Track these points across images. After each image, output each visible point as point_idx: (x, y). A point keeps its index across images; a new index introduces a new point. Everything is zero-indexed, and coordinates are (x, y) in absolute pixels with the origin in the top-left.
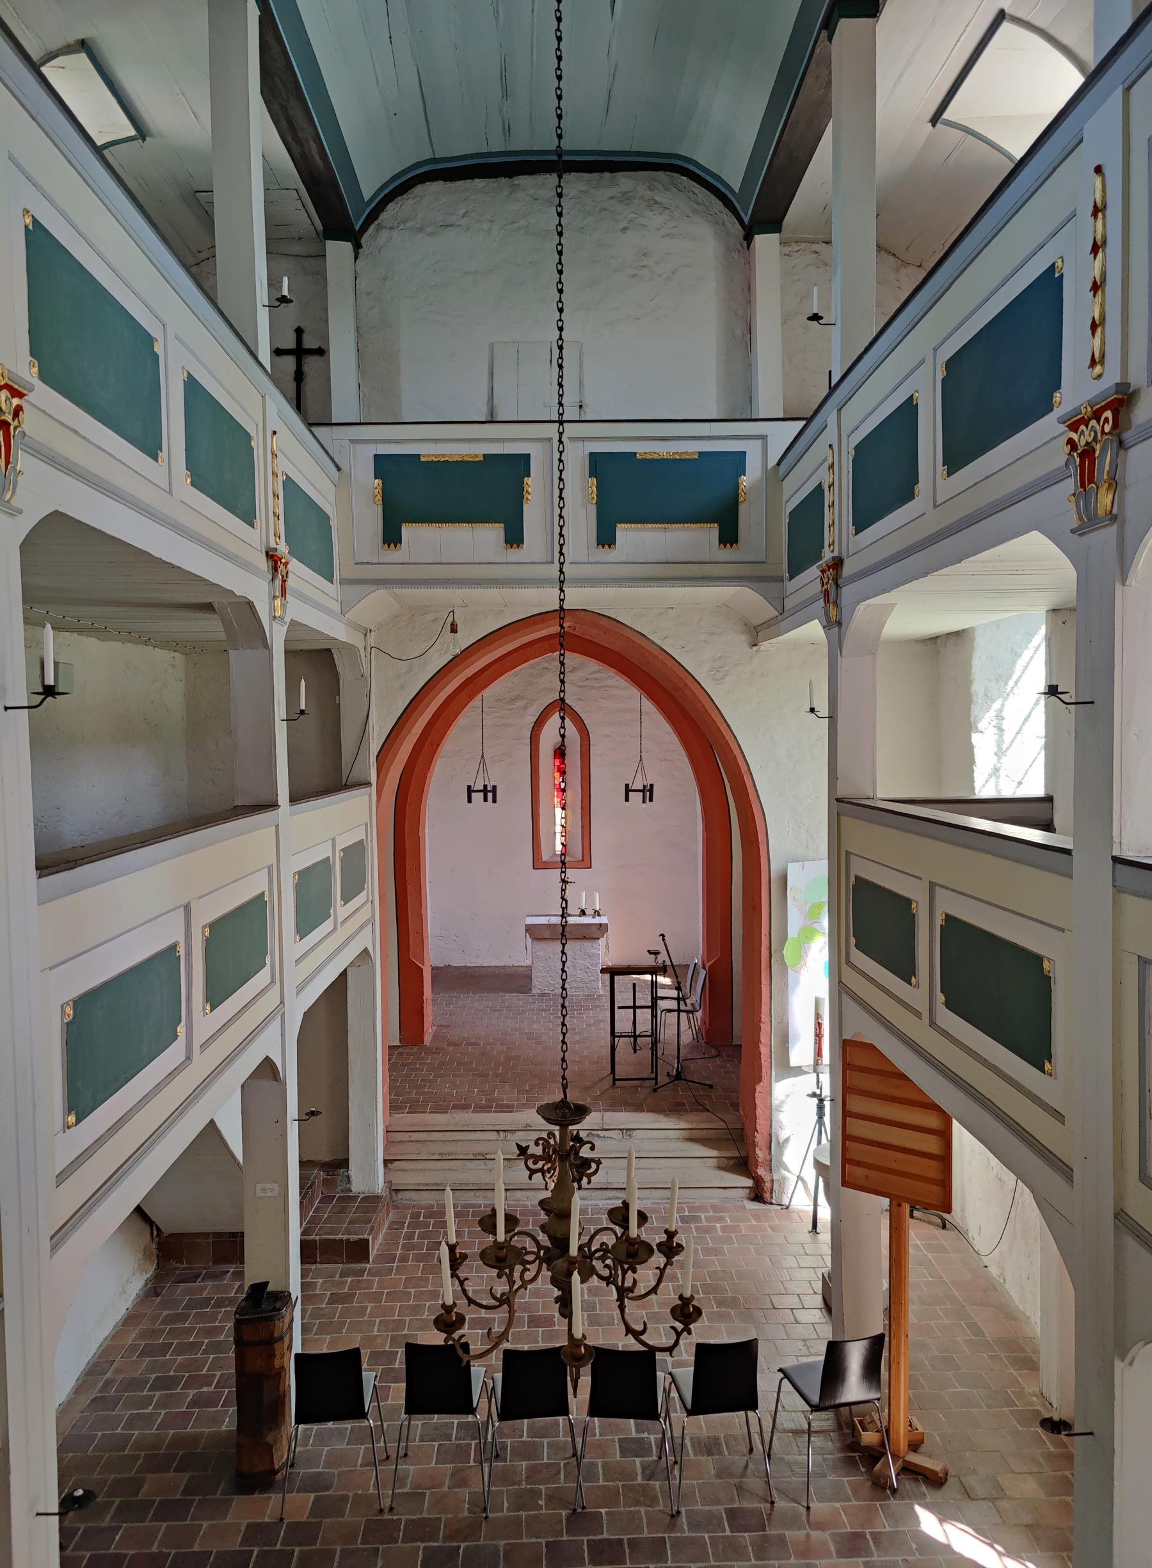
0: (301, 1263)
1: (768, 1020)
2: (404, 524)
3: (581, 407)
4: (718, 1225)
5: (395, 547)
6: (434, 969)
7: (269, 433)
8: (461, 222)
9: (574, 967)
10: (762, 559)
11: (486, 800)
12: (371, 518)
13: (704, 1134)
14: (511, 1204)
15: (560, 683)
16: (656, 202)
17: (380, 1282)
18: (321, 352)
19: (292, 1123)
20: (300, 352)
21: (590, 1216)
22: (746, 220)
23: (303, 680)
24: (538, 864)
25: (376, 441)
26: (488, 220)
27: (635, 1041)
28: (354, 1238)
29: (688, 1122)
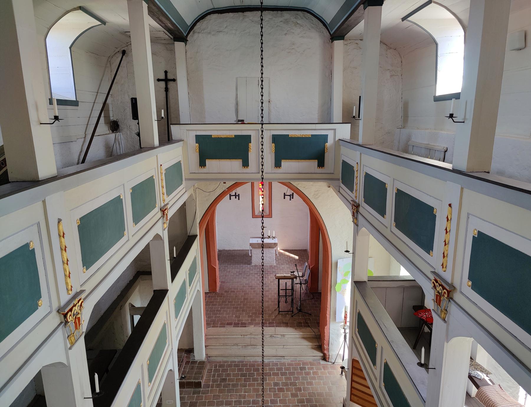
0: (180, 388)
1: (330, 307)
2: (207, 160)
3: (269, 102)
4: (311, 371)
5: (204, 167)
6: (219, 251)
7: (159, 166)
8: (225, 30)
9: (266, 257)
10: (332, 172)
11: (236, 198)
12: (195, 157)
13: (308, 336)
14: (246, 361)
15: (262, 289)
16: (298, 24)
17: (206, 397)
18: (174, 80)
19: (177, 381)
20: (166, 80)
21: (271, 367)
22: (332, 33)
23: (175, 247)
24: (254, 216)
25: (196, 130)
26: (235, 29)
27: (286, 291)
28: (197, 381)
29: (303, 332)
